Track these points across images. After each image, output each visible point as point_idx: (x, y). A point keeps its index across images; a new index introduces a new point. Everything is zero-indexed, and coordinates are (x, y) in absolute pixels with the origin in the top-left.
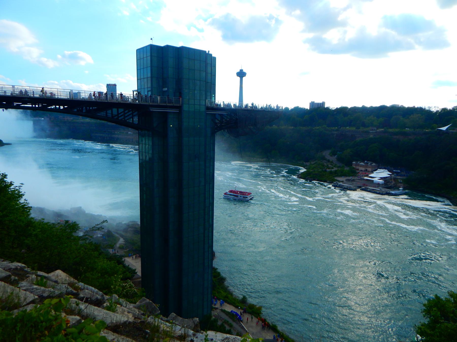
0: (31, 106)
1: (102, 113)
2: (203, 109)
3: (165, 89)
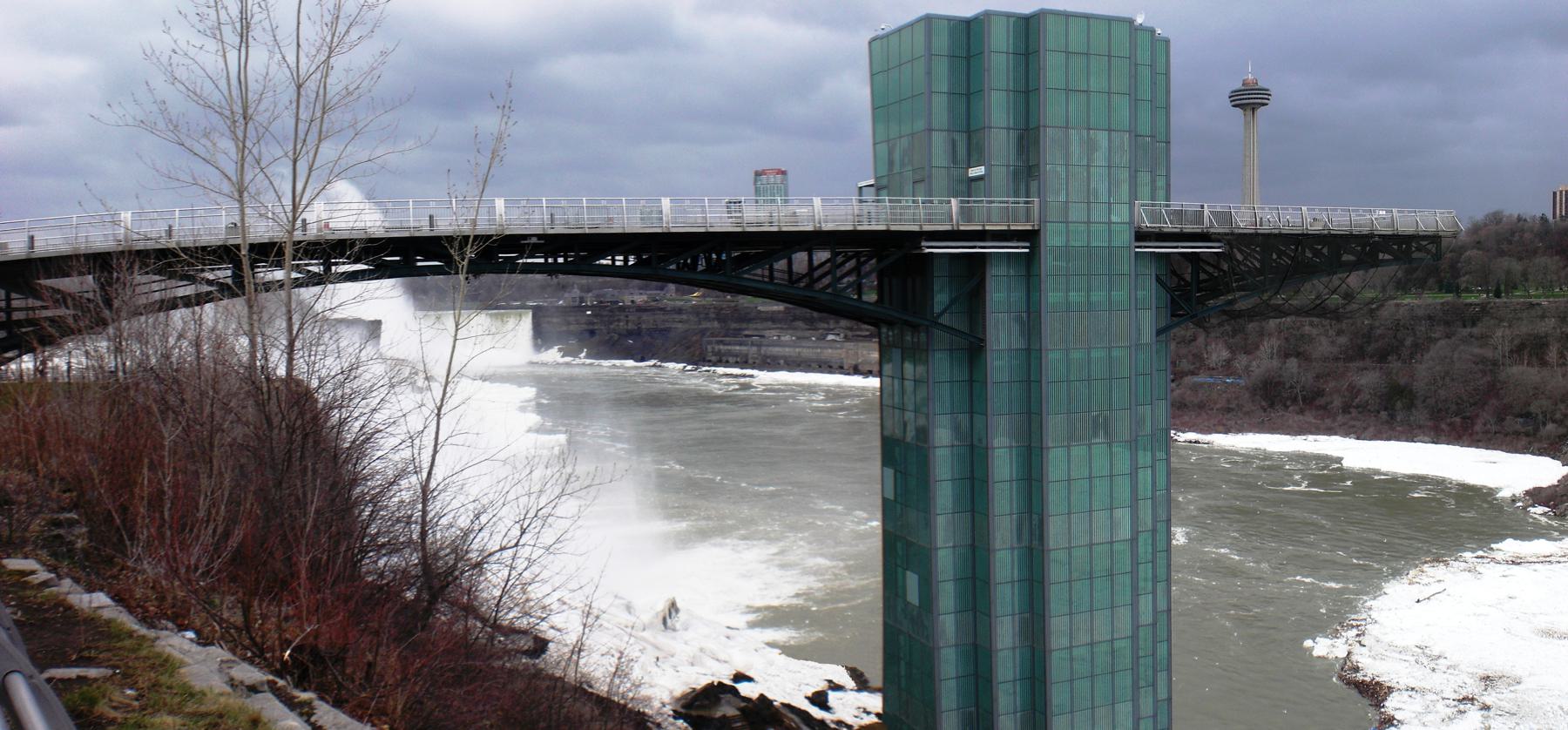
0: (542, 260)
1: (759, 271)
2: (1125, 237)
3: (975, 172)
